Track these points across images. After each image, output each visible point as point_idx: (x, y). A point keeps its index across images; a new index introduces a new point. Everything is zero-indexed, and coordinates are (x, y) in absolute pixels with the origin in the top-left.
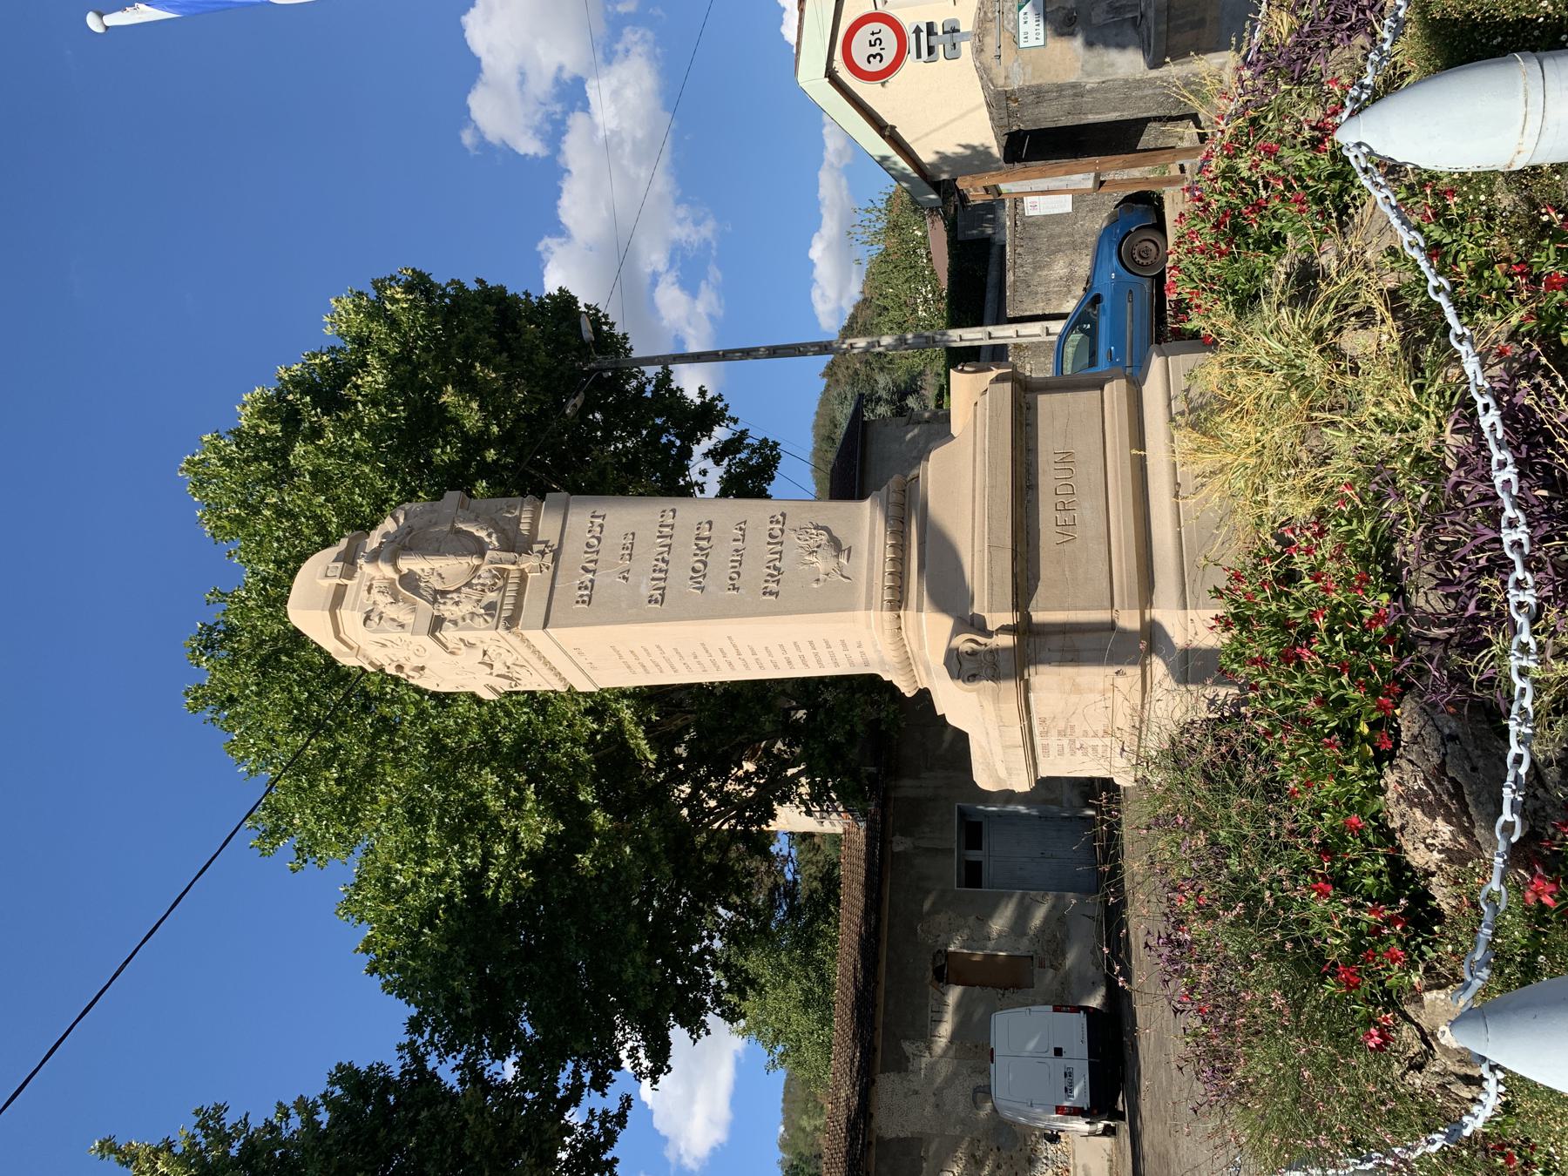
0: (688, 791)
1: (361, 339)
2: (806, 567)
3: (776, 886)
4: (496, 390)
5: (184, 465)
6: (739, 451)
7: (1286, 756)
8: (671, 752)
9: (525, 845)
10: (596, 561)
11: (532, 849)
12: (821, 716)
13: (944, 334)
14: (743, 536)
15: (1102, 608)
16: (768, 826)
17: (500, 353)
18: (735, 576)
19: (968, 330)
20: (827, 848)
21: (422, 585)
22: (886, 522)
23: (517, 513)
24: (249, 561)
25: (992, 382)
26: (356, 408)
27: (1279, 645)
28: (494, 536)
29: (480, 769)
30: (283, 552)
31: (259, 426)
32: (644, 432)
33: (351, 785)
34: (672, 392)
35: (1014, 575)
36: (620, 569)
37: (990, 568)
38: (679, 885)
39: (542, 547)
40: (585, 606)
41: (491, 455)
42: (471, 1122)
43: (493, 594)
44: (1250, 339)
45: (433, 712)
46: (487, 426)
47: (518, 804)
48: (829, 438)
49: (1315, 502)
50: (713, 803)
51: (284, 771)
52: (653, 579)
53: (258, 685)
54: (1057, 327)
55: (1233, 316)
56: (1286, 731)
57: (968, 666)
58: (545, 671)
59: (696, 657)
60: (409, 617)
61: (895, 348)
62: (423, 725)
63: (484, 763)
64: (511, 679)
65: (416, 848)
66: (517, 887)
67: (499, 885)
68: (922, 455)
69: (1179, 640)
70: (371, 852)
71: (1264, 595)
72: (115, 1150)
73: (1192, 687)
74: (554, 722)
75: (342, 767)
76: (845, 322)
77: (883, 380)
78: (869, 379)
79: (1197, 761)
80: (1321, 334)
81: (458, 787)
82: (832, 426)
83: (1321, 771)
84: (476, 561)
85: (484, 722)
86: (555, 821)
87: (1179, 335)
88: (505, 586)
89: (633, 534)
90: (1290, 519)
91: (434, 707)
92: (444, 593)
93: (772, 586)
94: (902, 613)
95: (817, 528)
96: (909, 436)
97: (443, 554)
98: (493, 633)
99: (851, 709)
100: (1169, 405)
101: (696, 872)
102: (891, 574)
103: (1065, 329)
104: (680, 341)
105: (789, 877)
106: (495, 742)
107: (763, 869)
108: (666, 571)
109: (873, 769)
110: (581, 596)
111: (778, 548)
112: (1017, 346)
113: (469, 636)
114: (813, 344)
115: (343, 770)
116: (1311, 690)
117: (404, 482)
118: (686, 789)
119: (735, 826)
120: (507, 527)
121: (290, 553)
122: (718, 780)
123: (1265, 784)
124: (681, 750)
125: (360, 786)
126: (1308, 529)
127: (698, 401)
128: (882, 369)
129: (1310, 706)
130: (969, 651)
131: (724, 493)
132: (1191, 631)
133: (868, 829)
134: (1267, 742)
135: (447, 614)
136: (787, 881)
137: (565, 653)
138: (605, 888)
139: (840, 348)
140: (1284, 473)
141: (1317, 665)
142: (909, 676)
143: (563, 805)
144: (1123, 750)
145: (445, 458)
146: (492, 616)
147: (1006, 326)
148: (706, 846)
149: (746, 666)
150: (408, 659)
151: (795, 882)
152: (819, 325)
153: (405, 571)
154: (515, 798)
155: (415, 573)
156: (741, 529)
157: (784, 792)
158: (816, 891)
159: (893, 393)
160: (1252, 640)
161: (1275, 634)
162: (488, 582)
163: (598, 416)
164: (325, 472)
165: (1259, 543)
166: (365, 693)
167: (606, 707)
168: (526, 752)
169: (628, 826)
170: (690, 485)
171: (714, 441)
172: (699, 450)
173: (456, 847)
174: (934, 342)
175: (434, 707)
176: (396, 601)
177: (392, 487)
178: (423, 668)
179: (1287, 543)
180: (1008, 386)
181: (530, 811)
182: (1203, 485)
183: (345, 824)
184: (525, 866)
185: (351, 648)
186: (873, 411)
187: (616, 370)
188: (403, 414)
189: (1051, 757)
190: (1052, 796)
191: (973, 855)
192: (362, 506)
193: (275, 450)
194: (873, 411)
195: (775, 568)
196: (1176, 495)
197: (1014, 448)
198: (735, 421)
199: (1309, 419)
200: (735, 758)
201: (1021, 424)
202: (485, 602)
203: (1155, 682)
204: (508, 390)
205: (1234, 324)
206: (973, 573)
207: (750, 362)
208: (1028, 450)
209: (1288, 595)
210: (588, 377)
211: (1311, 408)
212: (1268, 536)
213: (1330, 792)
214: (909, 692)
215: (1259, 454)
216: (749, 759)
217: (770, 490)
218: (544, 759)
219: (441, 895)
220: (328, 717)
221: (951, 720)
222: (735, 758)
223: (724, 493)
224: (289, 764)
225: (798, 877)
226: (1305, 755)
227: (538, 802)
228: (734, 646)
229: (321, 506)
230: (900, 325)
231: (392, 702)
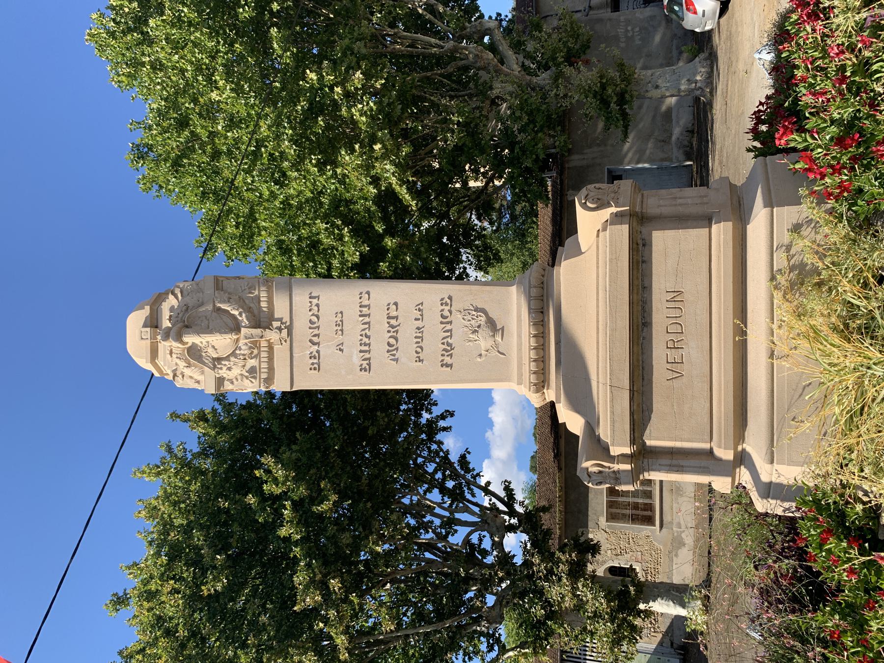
5: (87, 37)
18: (419, 350)
21: (204, 354)
23: (256, 293)
28: (244, 315)
35: (632, 414)
37: (612, 407)
40: (316, 372)
42: (349, 400)
43: (253, 361)
47: (341, 238)
72: (179, 417)
88: (259, 353)
92: (219, 360)
93: (447, 360)
94: (545, 391)
95: (477, 310)
99: (536, 145)
110: (313, 364)
120: (252, 305)
135: (225, 375)
146: (255, 378)
154: (338, 234)
155: (197, 345)
156: (420, 310)
175: (278, 190)
190: (666, 156)
196: (772, 355)
201: (638, 262)
202: (248, 367)
208: (644, 288)
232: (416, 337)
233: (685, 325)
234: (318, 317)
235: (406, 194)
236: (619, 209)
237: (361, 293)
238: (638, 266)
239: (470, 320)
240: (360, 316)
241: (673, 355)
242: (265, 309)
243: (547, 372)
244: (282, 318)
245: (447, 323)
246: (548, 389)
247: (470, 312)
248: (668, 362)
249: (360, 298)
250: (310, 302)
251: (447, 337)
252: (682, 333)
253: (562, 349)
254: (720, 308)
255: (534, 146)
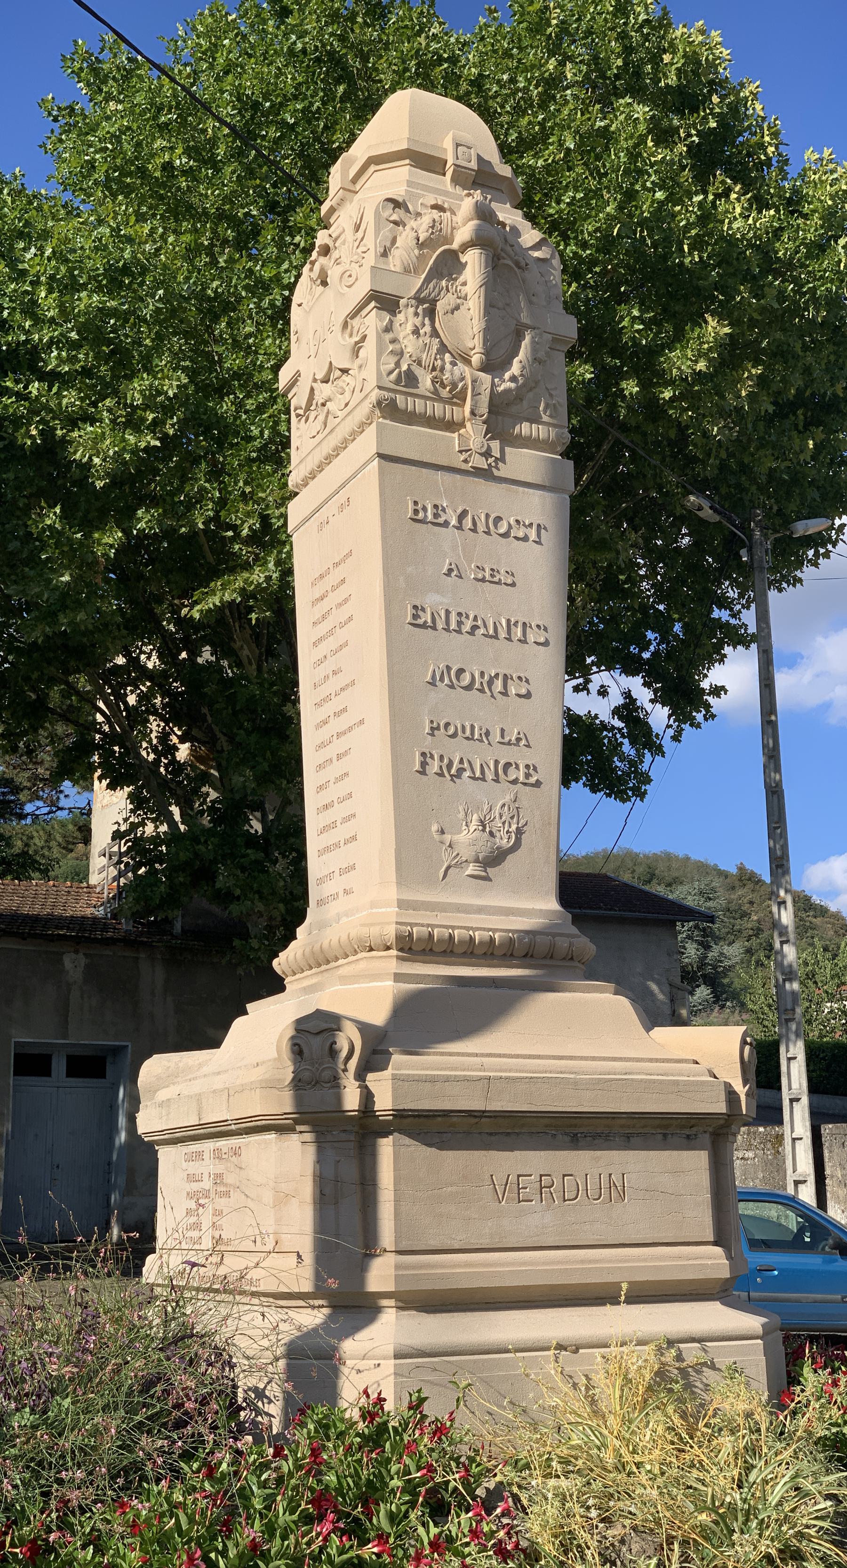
0: (150, 665)
1: (798, 203)
2: (462, 815)
3: (16, 790)
4: (722, 397)
6: (632, 743)
7: (178, 1497)
8: (205, 641)
9: (75, 434)
10: (474, 530)
11: (70, 442)
12: (253, 854)
13: (797, 1035)
14: (509, 743)
15: (398, 1239)
16: (100, 779)
17: (774, 403)
18: (451, 730)
19: (804, 1069)
20: (68, 862)
21: (444, 283)
22: (527, 932)
23: (545, 418)
24: (482, 39)
25: (728, 1086)
26: (697, 193)
27: (339, 1490)
28: (513, 385)
29: (184, 369)
30: (495, 88)
31: (674, 53)
32: (661, 607)
33: (163, 185)
34: (719, 648)
35: (446, 1114)
36: (463, 565)
38: (19, 652)
39: (496, 453)
40: (410, 514)
41: (631, 387)
43: (429, 383)
44: (786, 1454)
45: (265, 304)
46: (671, 383)
47: (134, 423)
48: (653, 875)
49: (549, 1547)
50: (132, 700)
51: (184, 88)
52: (448, 612)
53: (304, 51)
54: (807, 1195)
55: (822, 1433)
56: (212, 1497)
57: (316, 1044)
58: (318, 457)
59: (335, 673)
60: (398, 263)
61: (779, 965)
62: (246, 288)
63: (192, 374)
64: (308, 409)
65: (73, 277)
66: (17, 422)
67: (21, 396)
68: (623, 987)
69: (349, 1346)
70: (69, 213)
71: (413, 1468)
73: (282, 1363)
74: (250, 473)
75: (187, 172)
76: (816, 899)
77: (734, 952)
78: (735, 934)
79: (173, 1367)
80: (793, 1558)
81: (159, 337)
82: (668, 879)
83: (156, 1546)
84: (476, 359)
85: (251, 376)
86: (108, 474)
87: (794, 1358)
88: (440, 399)
89: (513, 585)
90: (524, 1509)
91: (272, 305)
92: (431, 313)
93: (434, 766)
95: (519, 832)
96: (654, 987)
97: (487, 312)
98: (372, 382)
99: (261, 898)
100: (693, 1340)
101: (35, 676)
102: (451, 937)
103: (804, 1205)
104: (793, 662)
105: (29, 808)
106: (221, 390)
107: (40, 770)
108: (459, 632)
109: (178, 927)
110: (425, 509)
111: (490, 776)
112: (780, 1138)
113: (369, 350)
114: (785, 847)
115: (184, 173)
116: (272, 1536)
117: (592, 262)
118: (152, 663)
119: (100, 732)
120: (525, 403)
121: (494, 97)
122: (164, 706)
123: (136, 1467)
124: (206, 655)
125: (161, 198)
126: (508, 1533)
127: (705, 685)
128: (749, 951)
129: (253, 1531)
130: (337, 1046)
131: (572, 719)
132: (362, 1364)
133: (95, 919)
134: (198, 1471)
135: (401, 317)
136: (23, 805)
137: (343, 486)
138: (13, 545)
139: (779, 886)
140: (591, 1502)
141: (309, 1544)
142: (303, 964)
143: (132, 486)
144: (194, 1265)
145: (625, 323)
146: (398, 381)
147: (808, 1124)
148: (71, 690)
149: (321, 746)
150: (337, 262)
151: (22, 816)
152: (814, 862)
153: (464, 259)
154: (143, 420)
155: (460, 273)
156: (518, 740)
157: (147, 800)
158: (9, 845)
159: (715, 967)
160: (348, 1450)
161: (356, 1484)
162: (447, 376)
163: (686, 540)
164: (607, 149)
165: (489, 1465)
166: (291, 208)
167: (266, 547)
168: (207, 432)
169: (99, 580)
170: (586, 673)
171: (648, 706)
172: (636, 685)
173: (74, 335)
174: (788, 1021)
175: (272, 305)
176: (421, 245)
177: (584, 245)
178: (324, 283)
179: (488, 1505)
180: (721, 1107)
181: (124, 440)
182: (575, 1386)
183: (107, 177)
184: (47, 433)
185: (354, 181)
186: (689, 937)
187: (751, 565)
188: (687, 260)
189: (185, 1165)
191: (59, 1066)
192: (558, 202)
193: (638, 74)
194: (689, 937)
195: (461, 771)
196: (560, 1347)
197: (631, 1115)
198: (676, 738)
199: (670, 1540)
200: (195, 732)
201: (666, 1127)
202: (418, 371)
203: (291, 1313)
204: (723, 413)
205: (810, 1434)
206: (451, 1054)
207: (761, 759)
208: (628, 1137)
209: (413, 1504)
210: (741, 528)
211: (685, 1543)
212: (499, 1478)
213: (123, 1558)
214: (279, 964)
215: (621, 1466)
216: (193, 751)
217: (578, 788)
218: (196, 461)
219: (5, 313)
220: (259, 154)
221: (238, 1024)
222: (195, 732)
223: (572, 719)
224: (193, 96)
225: (29, 820)
226: (178, 1523)
227: (135, 451)
228: (350, 729)
229: (561, 143)
230: (811, 976)
231: (280, 245)
232: (472, 727)
233: (576, 1205)
234: (506, 535)
235: (221, 601)
236: (743, 1098)
237: (546, 629)
238: (659, 1127)
239: (501, 816)
240: (508, 621)
241: (530, 1184)
242: (517, 430)
243: (427, 958)
244: (504, 462)
245: (496, 773)
246: (398, 958)
247: (515, 819)
248: (519, 1176)
249: (538, 626)
250: (531, 525)
251: (473, 772)
252: (565, 1201)
253: (484, 990)
254: (610, 1261)
255: (259, 892)
